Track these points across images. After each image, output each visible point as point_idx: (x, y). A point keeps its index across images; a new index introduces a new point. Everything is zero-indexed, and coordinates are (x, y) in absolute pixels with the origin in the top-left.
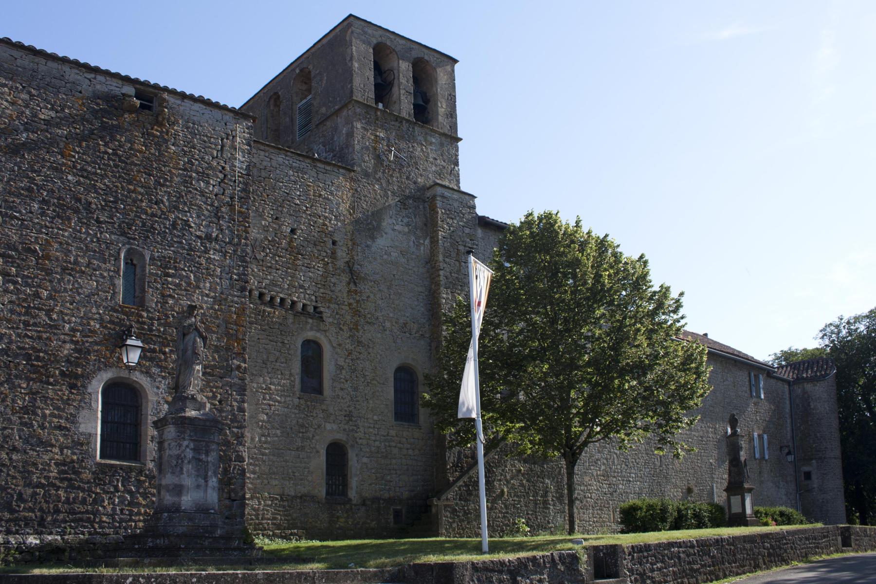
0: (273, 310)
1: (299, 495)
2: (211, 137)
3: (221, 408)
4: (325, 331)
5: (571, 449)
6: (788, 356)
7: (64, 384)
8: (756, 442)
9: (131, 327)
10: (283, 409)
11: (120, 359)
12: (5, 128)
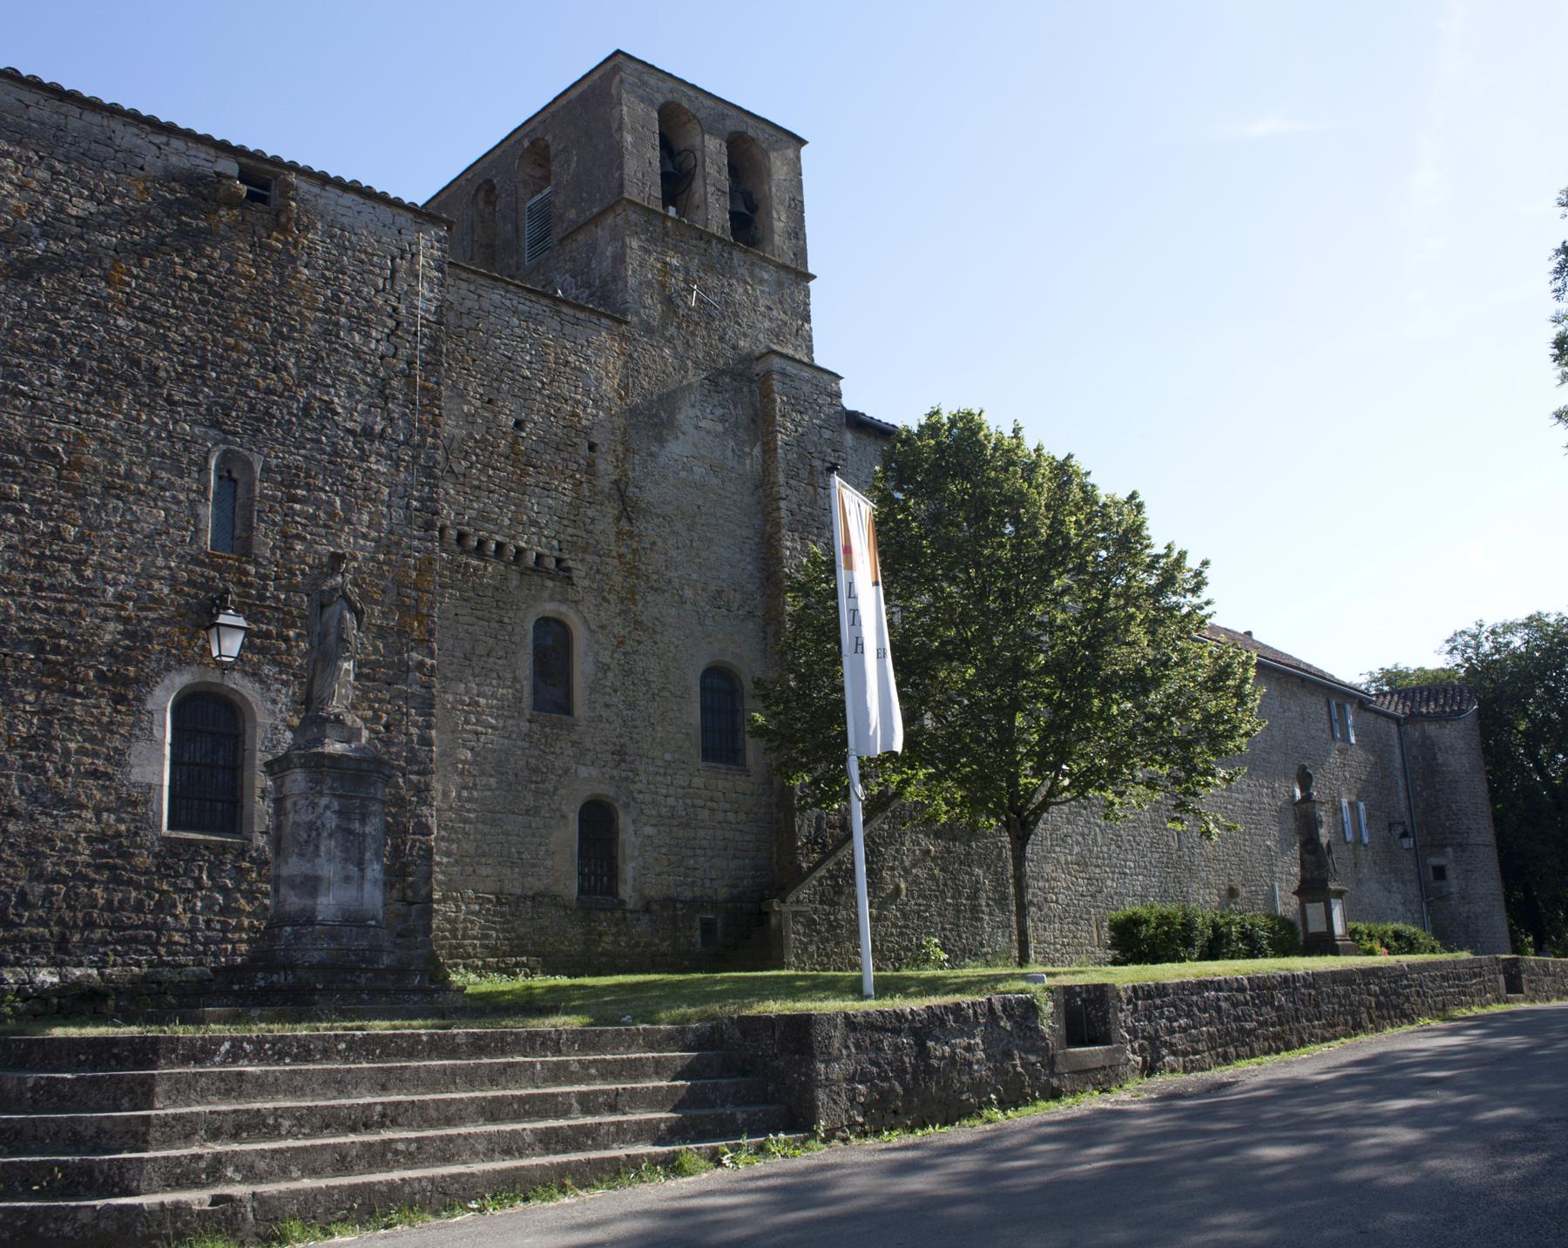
0: (482, 564)
1: (530, 893)
2: (373, 255)
3: (389, 738)
4: (576, 602)
5: (1019, 815)
6: (1394, 680)
7: (103, 696)
8: (1346, 815)
9: (227, 591)
10: (501, 741)
11: (206, 651)
12: (7, 232)
